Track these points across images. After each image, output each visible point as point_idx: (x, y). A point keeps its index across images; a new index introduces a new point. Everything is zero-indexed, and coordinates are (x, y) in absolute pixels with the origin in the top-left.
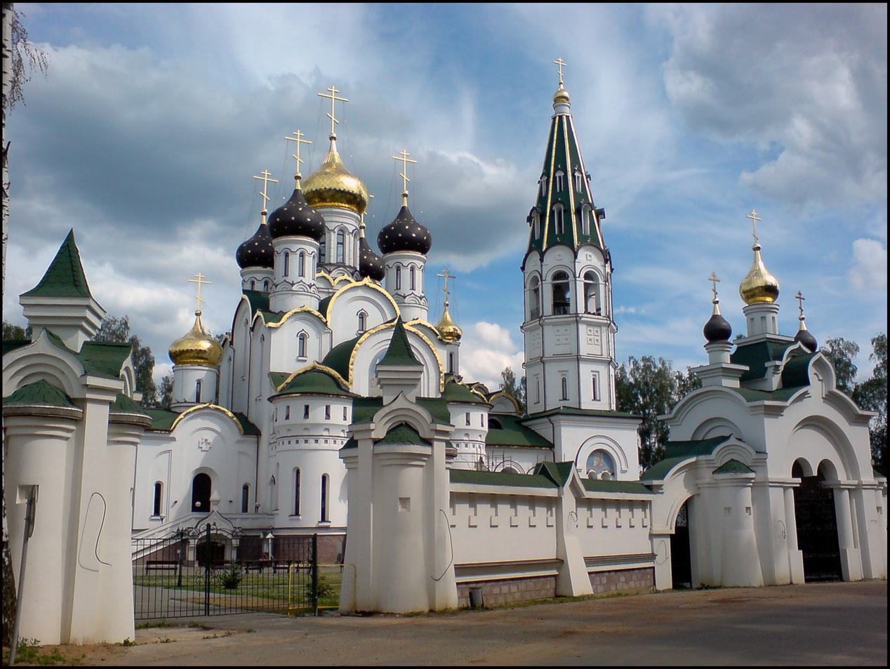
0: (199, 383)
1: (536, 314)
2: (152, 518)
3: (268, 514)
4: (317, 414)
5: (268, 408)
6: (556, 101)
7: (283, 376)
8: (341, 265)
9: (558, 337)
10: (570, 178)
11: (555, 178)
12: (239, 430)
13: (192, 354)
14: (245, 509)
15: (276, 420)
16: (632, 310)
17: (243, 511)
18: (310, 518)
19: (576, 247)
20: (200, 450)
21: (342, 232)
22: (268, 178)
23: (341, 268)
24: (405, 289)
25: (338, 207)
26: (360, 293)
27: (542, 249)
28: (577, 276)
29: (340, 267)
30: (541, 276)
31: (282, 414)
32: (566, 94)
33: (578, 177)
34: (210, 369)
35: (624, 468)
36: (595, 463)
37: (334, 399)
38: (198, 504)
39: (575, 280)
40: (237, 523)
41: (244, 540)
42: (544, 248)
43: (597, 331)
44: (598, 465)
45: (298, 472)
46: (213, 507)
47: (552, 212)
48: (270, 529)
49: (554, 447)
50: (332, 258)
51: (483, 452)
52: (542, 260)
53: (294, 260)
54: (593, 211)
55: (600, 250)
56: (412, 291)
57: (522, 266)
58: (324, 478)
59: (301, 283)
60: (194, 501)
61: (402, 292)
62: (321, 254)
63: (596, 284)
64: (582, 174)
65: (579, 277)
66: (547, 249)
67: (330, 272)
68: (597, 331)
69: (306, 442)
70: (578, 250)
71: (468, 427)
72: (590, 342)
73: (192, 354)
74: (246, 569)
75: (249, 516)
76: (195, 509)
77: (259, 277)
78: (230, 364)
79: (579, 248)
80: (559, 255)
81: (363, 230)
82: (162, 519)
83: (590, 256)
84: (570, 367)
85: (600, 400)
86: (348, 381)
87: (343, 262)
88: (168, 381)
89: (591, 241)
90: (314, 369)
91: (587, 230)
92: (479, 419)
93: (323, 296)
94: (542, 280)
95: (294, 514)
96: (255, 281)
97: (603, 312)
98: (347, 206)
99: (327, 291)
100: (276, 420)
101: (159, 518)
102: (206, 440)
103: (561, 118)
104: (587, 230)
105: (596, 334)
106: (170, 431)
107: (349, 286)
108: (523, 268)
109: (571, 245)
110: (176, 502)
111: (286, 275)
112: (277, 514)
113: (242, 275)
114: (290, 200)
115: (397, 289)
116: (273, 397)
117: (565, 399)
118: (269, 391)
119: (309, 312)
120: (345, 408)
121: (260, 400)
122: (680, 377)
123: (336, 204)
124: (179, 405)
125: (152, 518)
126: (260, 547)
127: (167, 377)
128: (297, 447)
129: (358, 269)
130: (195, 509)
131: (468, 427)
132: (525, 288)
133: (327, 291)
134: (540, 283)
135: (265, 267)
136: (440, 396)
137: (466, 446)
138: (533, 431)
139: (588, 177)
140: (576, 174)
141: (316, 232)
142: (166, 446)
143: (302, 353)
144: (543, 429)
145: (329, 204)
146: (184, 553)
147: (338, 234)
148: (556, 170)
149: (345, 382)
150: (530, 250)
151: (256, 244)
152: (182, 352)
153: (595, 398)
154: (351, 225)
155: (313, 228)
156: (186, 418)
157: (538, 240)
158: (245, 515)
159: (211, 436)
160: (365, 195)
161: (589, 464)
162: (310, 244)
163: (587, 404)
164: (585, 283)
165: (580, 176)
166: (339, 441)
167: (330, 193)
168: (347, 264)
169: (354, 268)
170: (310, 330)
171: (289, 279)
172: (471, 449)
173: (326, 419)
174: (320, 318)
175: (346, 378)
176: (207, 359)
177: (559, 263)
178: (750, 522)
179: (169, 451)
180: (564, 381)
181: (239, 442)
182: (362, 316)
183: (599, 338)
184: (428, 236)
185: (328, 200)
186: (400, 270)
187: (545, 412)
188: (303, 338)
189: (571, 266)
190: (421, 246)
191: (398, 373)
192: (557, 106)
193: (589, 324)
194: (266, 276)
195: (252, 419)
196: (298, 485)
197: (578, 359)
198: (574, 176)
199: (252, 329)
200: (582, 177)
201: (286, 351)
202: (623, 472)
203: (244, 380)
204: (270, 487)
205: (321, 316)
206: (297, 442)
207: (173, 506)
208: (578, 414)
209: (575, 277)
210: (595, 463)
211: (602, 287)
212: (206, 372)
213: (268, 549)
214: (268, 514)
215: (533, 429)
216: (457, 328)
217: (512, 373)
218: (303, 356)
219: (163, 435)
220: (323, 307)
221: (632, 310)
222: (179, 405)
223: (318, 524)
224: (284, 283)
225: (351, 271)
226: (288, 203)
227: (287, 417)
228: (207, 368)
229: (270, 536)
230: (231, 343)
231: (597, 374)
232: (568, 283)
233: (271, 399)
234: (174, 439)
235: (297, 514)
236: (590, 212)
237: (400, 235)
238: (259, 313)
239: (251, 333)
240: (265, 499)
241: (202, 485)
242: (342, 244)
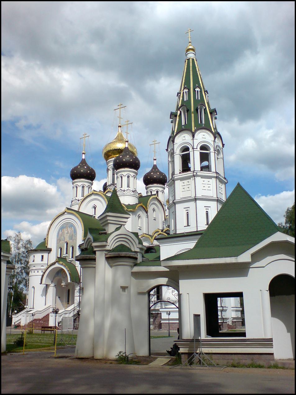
23: (112, 186)
33: (198, 91)
37: (40, 252)
55: (212, 132)
56: (129, 188)
57: (166, 148)
72: (183, 190)
79: (196, 131)
81: (84, 155)
95: (187, 225)
96: (152, 191)
109: (191, 131)
111: (122, 187)
139: (206, 92)
164: (200, 152)
166: (40, 271)
173: (41, 261)
178: (44, 371)
187: (197, 231)
189: (191, 142)
191: (225, 193)
198: (194, 90)
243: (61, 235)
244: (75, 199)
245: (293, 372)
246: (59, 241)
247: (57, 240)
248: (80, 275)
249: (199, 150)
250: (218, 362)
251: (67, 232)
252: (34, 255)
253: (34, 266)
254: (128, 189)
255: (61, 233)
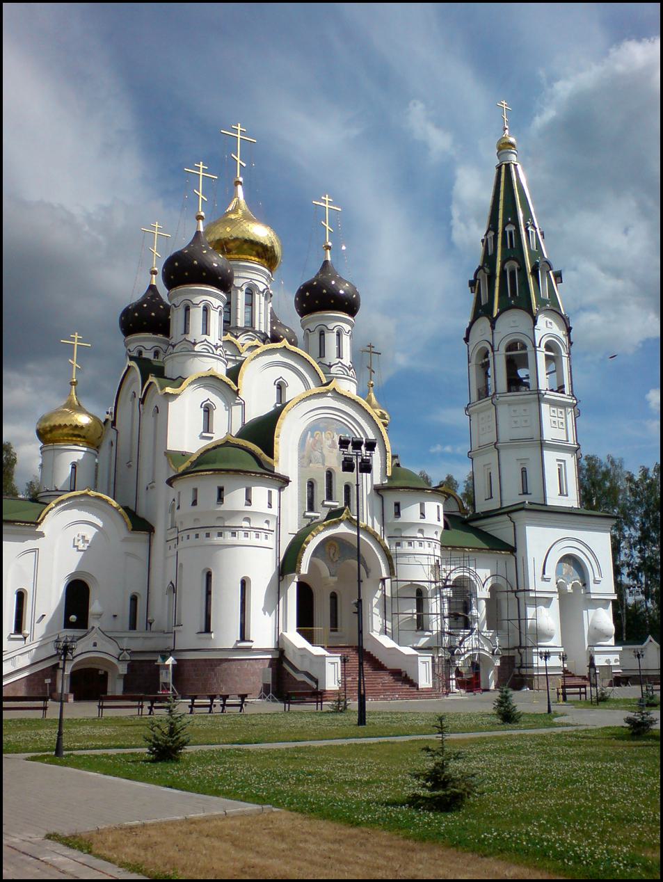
0: (74, 466)
1: (484, 393)
2: (12, 636)
3: (164, 632)
4: (235, 499)
5: (164, 494)
6: (500, 149)
7: (184, 455)
8: (250, 329)
9: (515, 419)
10: (523, 233)
11: (504, 233)
12: (127, 524)
13: (65, 431)
14: (133, 626)
15: (178, 508)
16: (448, 449)
17: (130, 629)
18: (226, 636)
19: (534, 312)
20: (76, 549)
21: (250, 292)
22: (158, 231)
23: (250, 333)
24: (331, 355)
25: (247, 260)
26: (277, 357)
27: (492, 314)
28: (537, 345)
29: (248, 331)
30: (492, 347)
31: (187, 499)
32: (512, 140)
33: (532, 232)
34: (90, 450)
35: (598, 577)
36: (564, 571)
38: (73, 618)
39: (536, 351)
40: (125, 644)
41: (132, 666)
42: (495, 315)
43: (561, 412)
44: (568, 574)
45: (209, 575)
46: (92, 622)
47: (503, 272)
48: (168, 651)
49: (516, 551)
50: (239, 321)
51: (438, 552)
52: (493, 328)
53: (197, 315)
54: (551, 272)
56: (338, 360)
58: (244, 583)
59: (205, 343)
60: (67, 616)
61: (327, 361)
62: (229, 307)
63: (557, 357)
64: (536, 229)
65: (540, 346)
66: (499, 315)
67: (237, 337)
68: (561, 412)
69: (220, 535)
70: (537, 315)
71: (422, 521)
72: (553, 425)
73: (65, 431)
74: (149, 708)
75: (139, 635)
76: (68, 624)
77: (148, 345)
78: (111, 449)
79: (538, 313)
80: (514, 322)
82: (25, 638)
83: (551, 323)
84: (530, 453)
85: (567, 495)
86: (273, 458)
87: (252, 326)
88: (33, 488)
89: (553, 309)
90: (227, 443)
91: (545, 293)
92: (434, 511)
93: (231, 365)
94: (493, 351)
97: (567, 389)
98: (257, 259)
99: (233, 358)
100: (178, 508)
101: (21, 636)
102: (83, 537)
103: (508, 166)
104: (545, 293)
105: (560, 415)
106: (38, 524)
107: (258, 351)
108: (467, 340)
109: (529, 309)
110: (44, 616)
111: (186, 331)
112: (180, 631)
113: (126, 345)
114: (190, 243)
115: (320, 357)
116: (175, 478)
117: (525, 493)
118: (164, 473)
119: (214, 377)
120: (270, 492)
121: (152, 487)
122: (630, 479)
123: (244, 257)
124: (47, 494)
125: (12, 636)
126: (157, 675)
127: (31, 482)
128: (208, 541)
129: (269, 336)
130: (68, 624)
131: (422, 521)
132: (469, 362)
133: (233, 358)
134: (490, 354)
135: (155, 333)
136: (387, 482)
137: (421, 545)
138: (486, 532)
140: (530, 229)
141: (223, 282)
142: (31, 544)
143: (208, 427)
144: (500, 529)
145: (237, 256)
146: (54, 684)
147: (246, 293)
148: (505, 224)
149: (268, 459)
150: (476, 317)
151: (145, 305)
152: (54, 428)
153: (561, 494)
154: (261, 282)
155: (220, 276)
156: (58, 507)
157: (486, 305)
158: (133, 634)
159: (90, 533)
160: (278, 250)
161: (558, 572)
162: (217, 296)
163: (554, 499)
164: (546, 355)
165: (534, 232)
167: (238, 243)
168: (257, 329)
169: (265, 334)
170: (217, 400)
171: (190, 338)
172: (426, 549)
174: (229, 385)
175: (271, 454)
176: (84, 437)
177: (514, 330)
179: (35, 550)
180: (524, 471)
181: (125, 540)
182: (281, 387)
183: (563, 420)
184: (358, 296)
185: (234, 252)
186: (324, 334)
187: (501, 509)
188: (208, 410)
190: (350, 306)
192: (501, 154)
193: (553, 403)
194: (156, 344)
195: (142, 513)
196: (208, 593)
197: (542, 445)
198: (527, 232)
199: (142, 401)
200: (536, 233)
201: (186, 425)
202: (596, 582)
203: (130, 466)
204: (167, 596)
205: (231, 383)
206: (197, 536)
207: (38, 622)
208: (545, 512)
209: (534, 346)
210: (564, 571)
211: (565, 361)
212: (83, 453)
213: (166, 677)
214: (164, 632)
215: (485, 530)
216: (384, 412)
217: (427, 477)
218: (208, 432)
219: (27, 529)
220: (234, 374)
221: (448, 449)
222: (47, 494)
223: (236, 644)
224: (184, 342)
225: (262, 337)
226: (189, 246)
227: (195, 503)
228: (85, 449)
229: (170, 661)
230: (114, 423)
231: (562, 463)
232: (526, 354)
233: (170, 482)
234: (41, 535)
235: (208, 630)
236: (548, 272)
237: (325, 291)
238: (152, 379)
239: (141, 405)
240: (160, 609)
241: (77, 595)
242: (251, 305)
243: (314, 447)
244: (206, 340)
245: (5, 842)
246: (306, 461)
247: (301, 458)
248: (410, 583)
249: (544, 350)
250: (416, 855)
251: (329, 442)
252: (270, 489)
253: (248, 519)
254: (339, 362)
255: (311, 441)
